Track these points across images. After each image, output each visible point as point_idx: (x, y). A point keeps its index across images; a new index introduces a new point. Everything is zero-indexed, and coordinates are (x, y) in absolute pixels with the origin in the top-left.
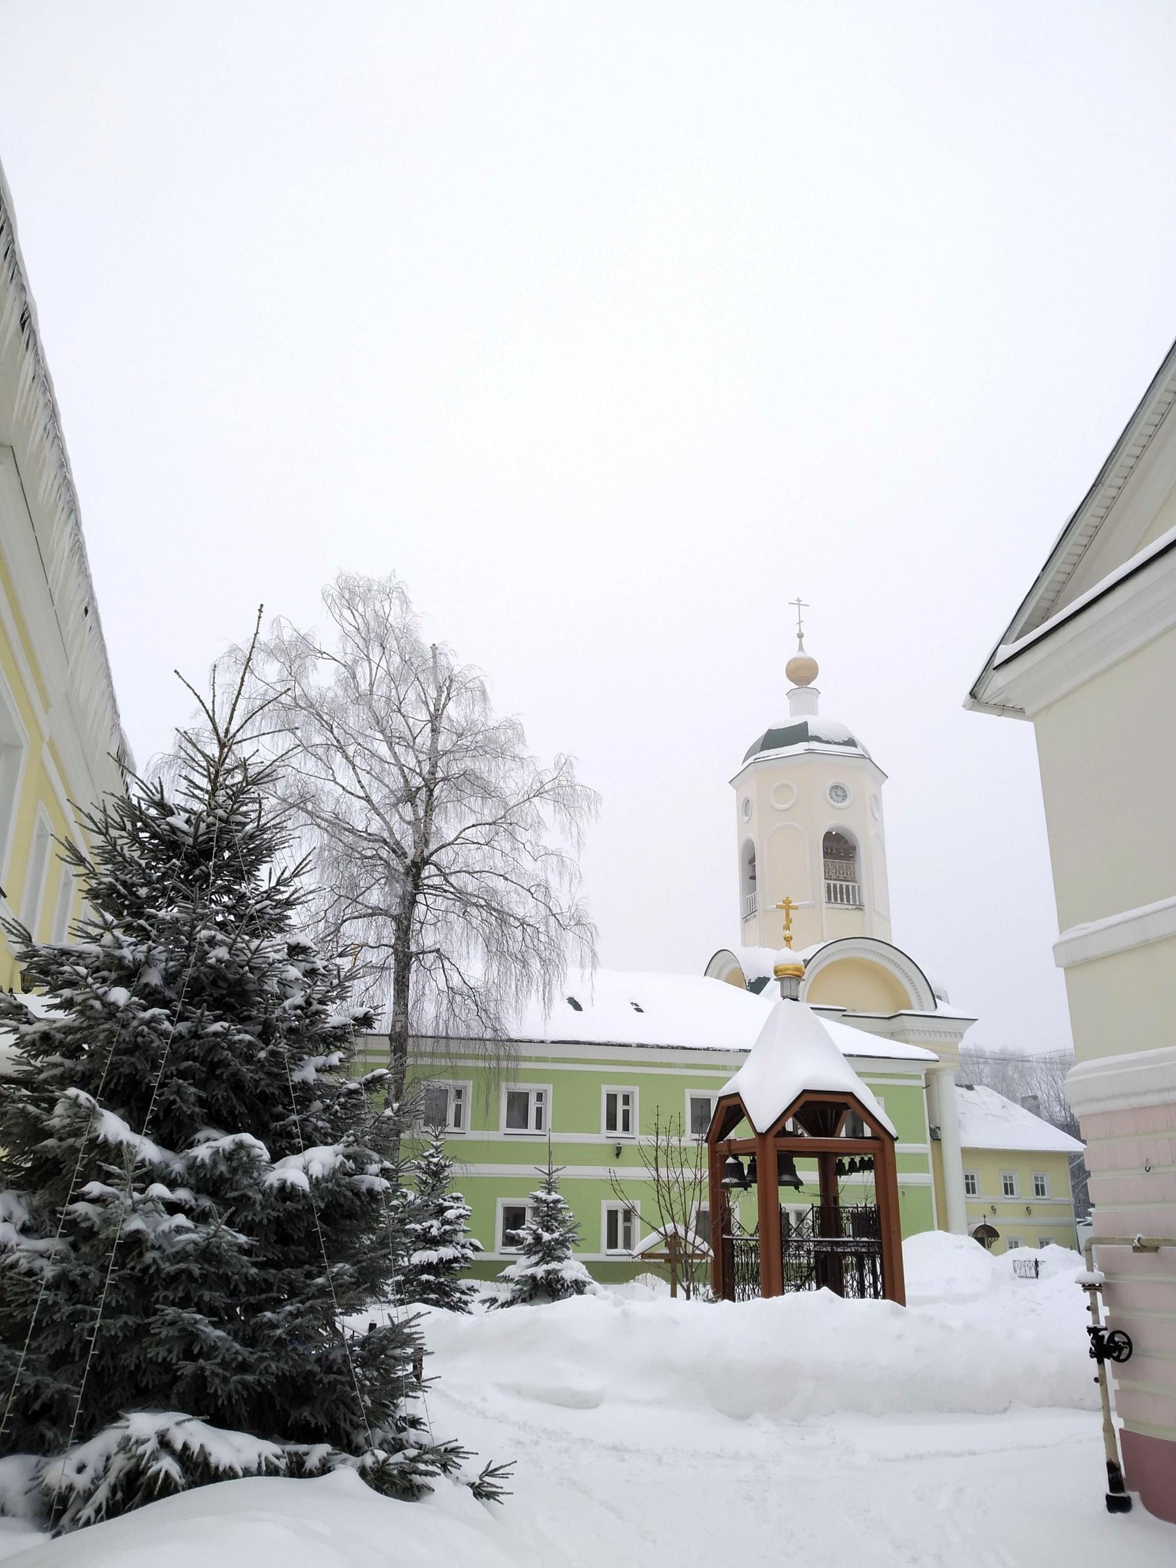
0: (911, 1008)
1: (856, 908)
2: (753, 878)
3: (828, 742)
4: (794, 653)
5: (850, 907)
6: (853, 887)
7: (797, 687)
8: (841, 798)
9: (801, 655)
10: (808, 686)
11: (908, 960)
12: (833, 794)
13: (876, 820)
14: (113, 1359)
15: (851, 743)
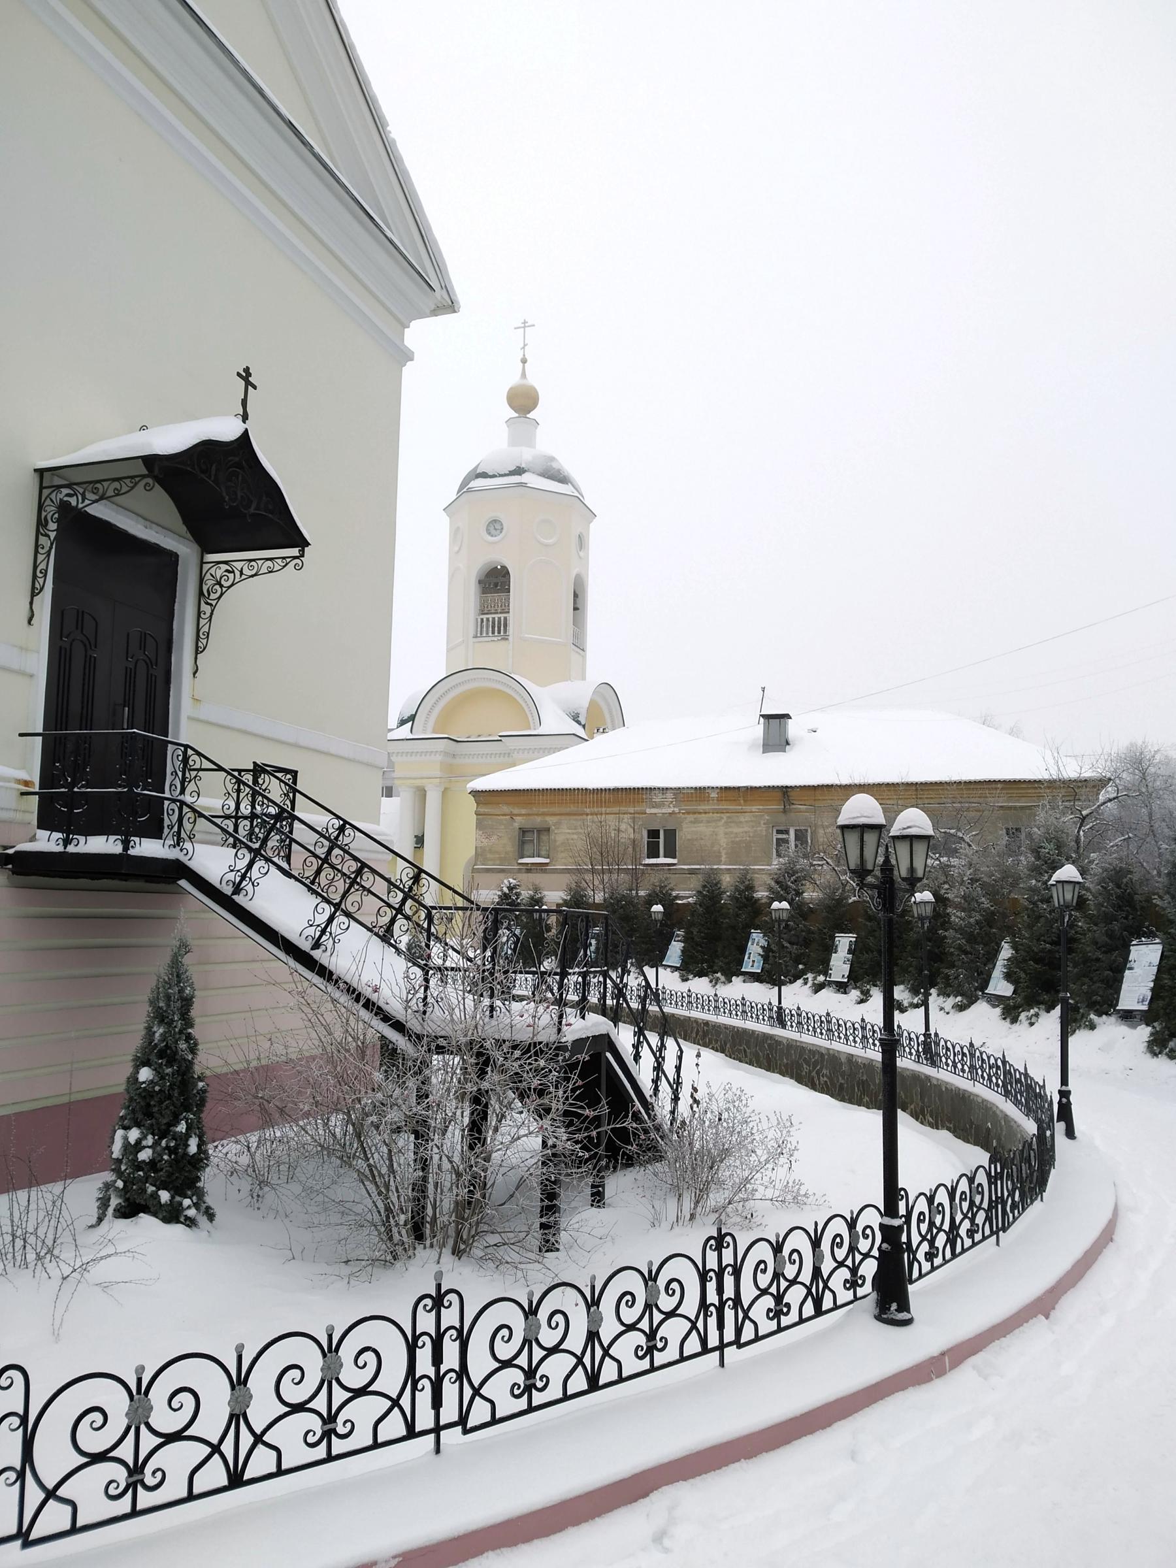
0: (529, 728)
1: (502, 639)
2: (576, 596)
3: (494, 476)
4: (514, 379)
5: (496, 639)
6: (505, 619)
7: (517, 415)
8: (498, 531)
9: (524, 382)
10: (528, 416)
11: (424, 700)
12: (492, 528)
13: (580, 558)
14: (285, 1114)
15: (563, 479)
